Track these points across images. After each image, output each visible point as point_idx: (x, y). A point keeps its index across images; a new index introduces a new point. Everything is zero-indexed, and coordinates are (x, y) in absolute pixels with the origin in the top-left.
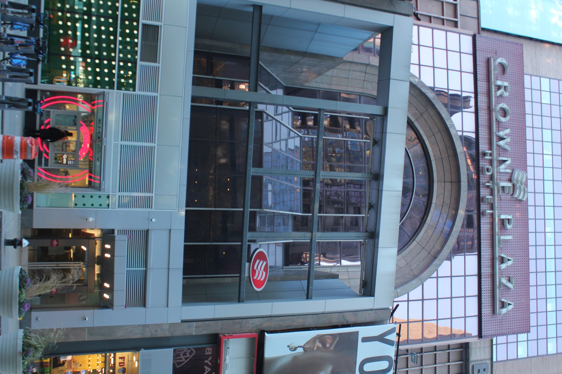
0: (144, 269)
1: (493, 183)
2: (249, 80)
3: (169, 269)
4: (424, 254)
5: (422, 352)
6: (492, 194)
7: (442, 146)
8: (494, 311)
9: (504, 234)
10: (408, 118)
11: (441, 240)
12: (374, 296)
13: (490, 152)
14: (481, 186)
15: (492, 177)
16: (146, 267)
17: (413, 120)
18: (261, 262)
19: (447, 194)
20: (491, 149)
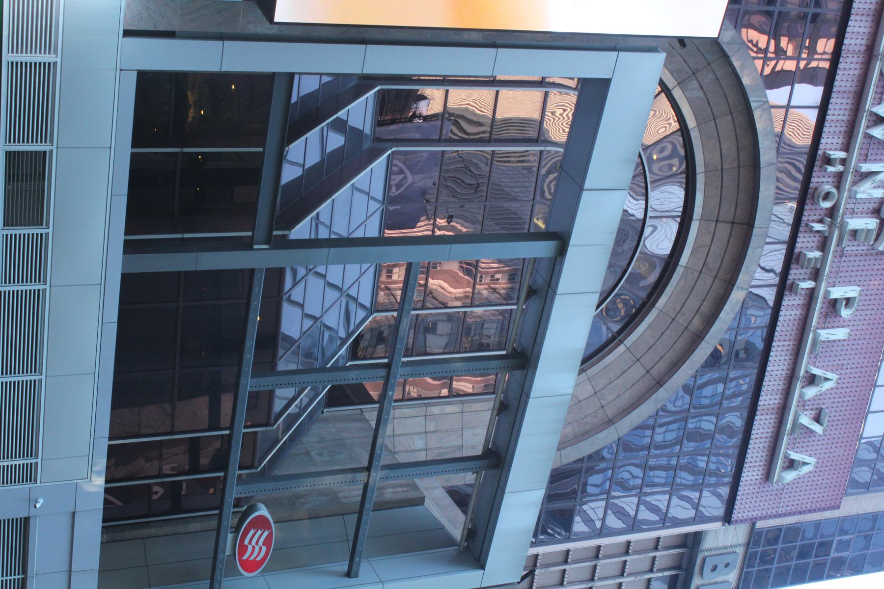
0: (21, 577)
1: (831, 226)
2: (253, 230)
3: (70, 571)
4: (637, 371)
5: (597, 557)
6: (823, 246)
7: (729, 146)
8: (768, 475)
9: (832, 324)
10: (661, 80)
11: (681, 344)
12: (483, 567)
13: (843, 155)
14: (801, 229)
15: (832, 212)
16: (25, 572)
17: (670, 82)
18: (259, 533)
19: (717, 248)
20: (847, 147)
